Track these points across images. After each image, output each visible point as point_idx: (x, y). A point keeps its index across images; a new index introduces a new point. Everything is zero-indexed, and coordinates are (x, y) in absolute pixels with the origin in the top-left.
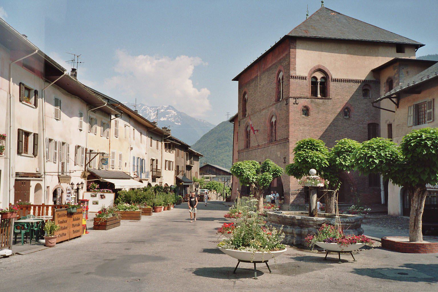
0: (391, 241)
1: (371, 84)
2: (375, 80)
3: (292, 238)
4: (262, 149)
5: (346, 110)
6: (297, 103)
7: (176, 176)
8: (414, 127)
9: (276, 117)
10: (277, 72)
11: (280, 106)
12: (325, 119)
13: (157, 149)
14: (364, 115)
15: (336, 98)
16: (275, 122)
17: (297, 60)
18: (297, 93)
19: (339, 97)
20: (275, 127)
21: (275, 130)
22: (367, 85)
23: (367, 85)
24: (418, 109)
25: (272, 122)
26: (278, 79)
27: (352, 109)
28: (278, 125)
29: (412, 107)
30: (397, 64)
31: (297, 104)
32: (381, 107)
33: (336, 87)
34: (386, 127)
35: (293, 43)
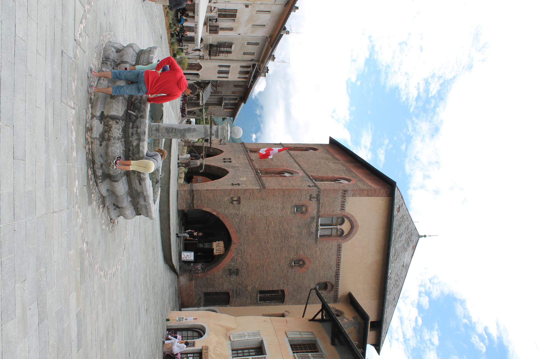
1: (334, 292)
2: (339, 297)
4: (248, 164)
5: (301, 263)
6: (312, 199)
7: (210, 82)
8: (286, 340)
10: (347, 177)
11: (306, 180)
12: (291, 236)
13: (245, 54)
14: (296, 284)
15: (317, 249)
17: (366, 198)
18: (324, 199)
19: (318, 253)
22: (333, 287)
23: (333, 287)
24: (338, 315)
25: (284, 174)
26: (339, 178)
27: (303, 269)
29: (312, 336)
30: (360, 319)
31: (310, 200)
32: (308, 305)
33: (331, 249)
34: (281, 312)
35: (386, 193)
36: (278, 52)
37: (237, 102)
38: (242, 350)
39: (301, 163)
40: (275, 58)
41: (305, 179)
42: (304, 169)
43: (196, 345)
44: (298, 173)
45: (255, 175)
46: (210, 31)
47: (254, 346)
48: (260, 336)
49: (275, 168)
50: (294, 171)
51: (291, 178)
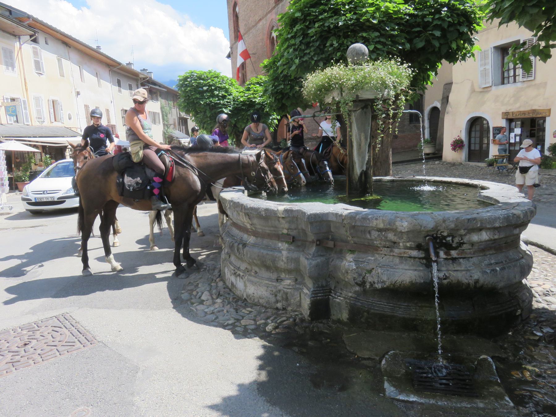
3: (297, 289)
25: (273, 37)
36: (123, 60)
39: (257, 18)
40: (129, 63)
42: (265, 13)
44: (272, 20)
46: (517, 81)
47: (500, 58)
48: (488, 51)
49: (265, 49)
50: (269, 25)
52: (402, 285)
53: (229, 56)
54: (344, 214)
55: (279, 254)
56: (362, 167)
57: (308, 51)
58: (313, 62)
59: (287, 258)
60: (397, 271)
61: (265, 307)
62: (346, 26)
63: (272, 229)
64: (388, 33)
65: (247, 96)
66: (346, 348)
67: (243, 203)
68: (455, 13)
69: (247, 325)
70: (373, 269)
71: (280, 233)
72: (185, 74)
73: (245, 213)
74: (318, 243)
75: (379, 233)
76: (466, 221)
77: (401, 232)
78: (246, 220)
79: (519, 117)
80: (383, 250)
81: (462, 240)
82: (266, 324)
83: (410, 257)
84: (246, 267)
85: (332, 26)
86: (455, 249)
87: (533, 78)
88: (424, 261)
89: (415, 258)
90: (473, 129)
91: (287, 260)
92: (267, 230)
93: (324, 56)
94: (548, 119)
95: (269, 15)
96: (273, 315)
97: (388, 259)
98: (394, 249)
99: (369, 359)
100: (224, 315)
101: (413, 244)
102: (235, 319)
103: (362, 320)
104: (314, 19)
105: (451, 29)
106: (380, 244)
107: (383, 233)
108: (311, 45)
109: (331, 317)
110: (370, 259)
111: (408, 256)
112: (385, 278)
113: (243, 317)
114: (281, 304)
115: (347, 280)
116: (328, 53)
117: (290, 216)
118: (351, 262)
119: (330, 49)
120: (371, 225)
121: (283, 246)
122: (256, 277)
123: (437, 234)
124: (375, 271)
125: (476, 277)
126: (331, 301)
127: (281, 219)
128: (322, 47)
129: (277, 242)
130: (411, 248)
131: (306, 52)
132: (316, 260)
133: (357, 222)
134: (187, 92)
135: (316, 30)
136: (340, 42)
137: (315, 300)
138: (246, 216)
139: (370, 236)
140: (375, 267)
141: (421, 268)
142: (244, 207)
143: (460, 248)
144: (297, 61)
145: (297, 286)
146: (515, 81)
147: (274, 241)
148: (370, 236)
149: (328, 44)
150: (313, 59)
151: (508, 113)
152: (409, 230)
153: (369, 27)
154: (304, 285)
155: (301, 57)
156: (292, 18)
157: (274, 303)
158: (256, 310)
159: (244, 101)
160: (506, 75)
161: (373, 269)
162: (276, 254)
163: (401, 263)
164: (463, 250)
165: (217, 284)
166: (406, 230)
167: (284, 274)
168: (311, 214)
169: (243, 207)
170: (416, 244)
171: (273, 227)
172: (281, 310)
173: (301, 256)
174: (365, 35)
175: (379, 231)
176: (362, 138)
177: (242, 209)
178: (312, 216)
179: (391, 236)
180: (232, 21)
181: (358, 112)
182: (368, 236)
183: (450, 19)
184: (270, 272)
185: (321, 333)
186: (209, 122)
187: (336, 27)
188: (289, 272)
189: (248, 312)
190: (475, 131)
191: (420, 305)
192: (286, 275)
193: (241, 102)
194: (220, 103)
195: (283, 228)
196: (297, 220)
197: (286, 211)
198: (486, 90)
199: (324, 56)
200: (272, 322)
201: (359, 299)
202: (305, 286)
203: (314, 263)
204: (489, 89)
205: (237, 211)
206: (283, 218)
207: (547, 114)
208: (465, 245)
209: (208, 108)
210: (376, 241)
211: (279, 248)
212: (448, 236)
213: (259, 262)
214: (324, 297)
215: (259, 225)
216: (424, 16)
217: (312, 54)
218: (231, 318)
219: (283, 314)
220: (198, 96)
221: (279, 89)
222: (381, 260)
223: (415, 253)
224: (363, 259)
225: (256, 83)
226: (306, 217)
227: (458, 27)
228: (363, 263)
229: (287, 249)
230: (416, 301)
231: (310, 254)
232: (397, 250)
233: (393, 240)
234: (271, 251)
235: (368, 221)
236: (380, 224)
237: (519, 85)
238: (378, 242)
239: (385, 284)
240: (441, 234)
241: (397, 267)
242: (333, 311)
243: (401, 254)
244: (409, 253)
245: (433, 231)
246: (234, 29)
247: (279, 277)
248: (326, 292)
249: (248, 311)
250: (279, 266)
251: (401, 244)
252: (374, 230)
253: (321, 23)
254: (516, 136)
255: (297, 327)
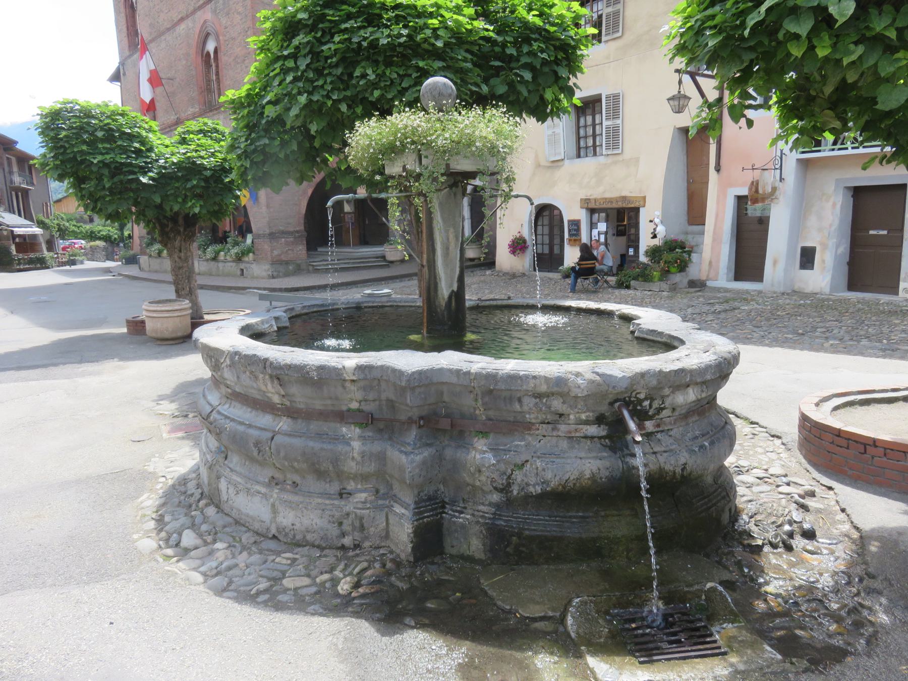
0: (411, 349)
3: (380, 508)
9: (217, 40)
16: (216, 51)
20: (217, 66)
21: (217, 74)
25: (208, 54)
28: (223, 58)
37: (14, 159)
38: (579, 138)
39: (176, 17)
41: (221, 7)
42: (191, 9)
43: (576, 218)
44: (205, 22)
45: (219, 113)
46: (598, 154)
49: (194, 73)
50: (200, 32)
51: (221, 38)
52: (578, 485)
53: (116, 77)
54: (472, 371)
55: (348, 448)
56: (451, 285)
57: (320, 83)
58: (330, 103)
59: (363, 454)
60: (569, 461)
61: (318, 547)
62: (391, 47)
63: (329, 402)
64: (457, 65)
65: (184, 154)
66: (495, 604)
67: (266, 356)
68: (551, 45)
69: (299, 588)
70: (527, 461)
71: (344, 408)
72: (53, 104)
73: (271, 377)
74: (422, 422)
75: (538, 400)
76: (673, 374)
77: (576, 397)
78: (273, 387)
79: (604, 206)
80: (540, 428)
81: (663, 403)
82: (335, 582)
83: (586, 437)
84: (271, 475)
85: (365, 44)
86: (651, 418)
87: (620, 151)
88: (607, 441)
89: (592, 438)
90: (540, 223)
91: (363, 457)
92: (318, 405)
93: (348, 93)
94: (641, 210)
95: (199, 13)
96: (339, 560)
97: (549, 442)
98: (559, 426)
99: (542, 619)
100: (244, 575)
101: (591, 415)
102: (269, 579)
103: (508, 549)
104: (330, 29)
105: (546, 69)
106: (537, 418)
107: (544, 400)
108: (326, 72)
109: (447, 551)
110: (517, 446)
111: (582, 435)
112: (549, 475)
113: (284, 573)
114: (351, 538)
115: (478, 483)
116: (358, 89)
117: (368, 377)
118: (484, 452)
119: (361, 83)
120: (525, 387)
121: (350, 432)
122: (296, 494)
123: (630, 397)
124: (531, 465)
125: (682, 460)
126: (446, 524)
127: (348, 384)
128: (346, 78)
129: (338, 425)
130: (587, 422)
131: (316, 84)
132: (420, 454)
133: (499, 384)
134: (61, 139)
135: (337, 46)
136: (379, 71)
137: (420, 524)
138: (272, 382)
139: (521, 406)
140: (529, 458)
141: (605, 454)
142: (271, 363)
143: (657, 417)
144: (303, 99)
145: (380, 502)
146: (595, 154)
147: (332, 425)
148: (521, 406)
149: (357, 73)
150: (329, 98)
151: (589, 199)
152: (589, 393)
153: (427, 51)
154: (395, 498)
155: (310, 93)
156: (286, 21)
157: (337, 537)
158: (302, 556)
159: (180, 161)
160: (582, 144)
161: (527, 461)
162: (340, 448)
163: (572, 448)
164: (662, 419)
165: (202, 512)
166: (586, 393)
167: (352, 483)
168: (413, 373)
169: (268, 364)
170: (597, 414)
171: (331, 398)
172: (350, 549)
173: (389, 447)
174: (421, 64)
175: (536, 397)
176: (451, 236)
177: (265, 368)
178: (415, 376)
179: (557, 404)
180: (123, 15)
181: (443, 192)
182: (517, 407)
183: (544, 56)
184: (325, 481)
185: (440, 583)
186: (107, 199)
187: (374, 44)
188: (365, 478)
189: (289, 562)
190: (543, 225)
191: (603, 513)
192: (357, 484)
193: (174, 164)
194: (131, 164)
195: (352, 400)
196: (379, 385)
197: (360, 368)
198: (556, 164)
199: (348, 93)
200: (345, 576)
201: (500, 515)
202: (396, 502)
203: (418, 458)
204: (560, 164)
205: (251, 372)
206: (353, 381)
207: (642, 203)
208: (664, 412)
209: (106, 172)
210: (529, 413)
211: (343, 436)
212: (646, 399)
213: (305, 466)
214: (435, 517)
215: (301, 396)
216: (504, 45)
217: (328, 87)
218: (260, 579)
219: (357, 555)
220: (84, 148)
221: (260, 145)
222: (538, 446)
223: (593, 430)
224: (505, 445)
225: (198, 131)
226: (404, 379)
227: (555, 68)
228: (507, 452)
229: (360, 437)
230: (596, 508)
231: (409, 444)
232: (564, 426)
233: (561, 411)
234: (330, 443)
235: (519, 381)
236: (541, 384)
237: (601, 160)
238: (532, 416)
239: (548, 485)
240: (636, 397)
241: (567, 455)
242: (448, 542)
243: (570, 432)
244: (584, 430)
245: (626, 392)
246: (128, 29)
247: (344, 489)
248: (436, 509)
249: (288, 559)
250: (346, 469)
251: (572, 417)
252: (527, 395)
253: (346, 36)
254: (599, 234)
255: (393, 579)
